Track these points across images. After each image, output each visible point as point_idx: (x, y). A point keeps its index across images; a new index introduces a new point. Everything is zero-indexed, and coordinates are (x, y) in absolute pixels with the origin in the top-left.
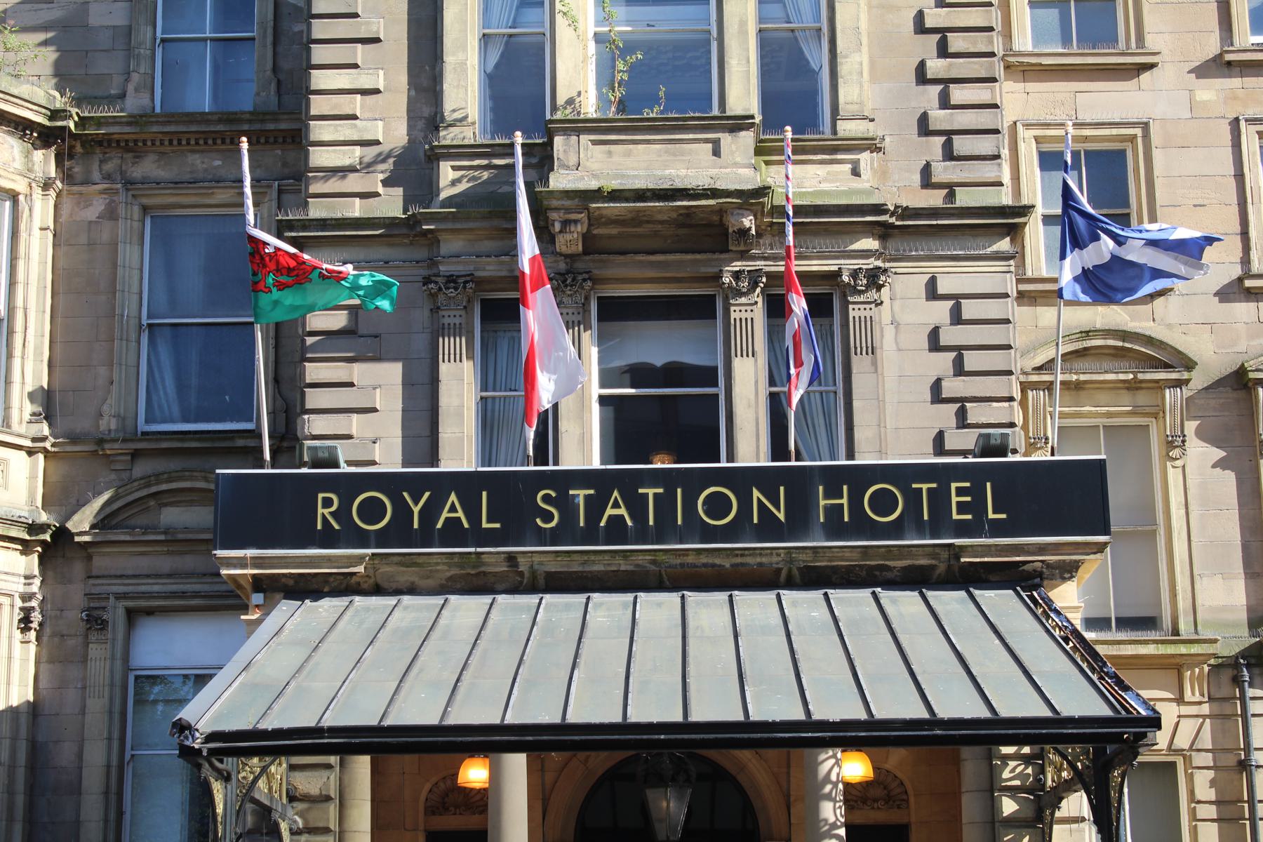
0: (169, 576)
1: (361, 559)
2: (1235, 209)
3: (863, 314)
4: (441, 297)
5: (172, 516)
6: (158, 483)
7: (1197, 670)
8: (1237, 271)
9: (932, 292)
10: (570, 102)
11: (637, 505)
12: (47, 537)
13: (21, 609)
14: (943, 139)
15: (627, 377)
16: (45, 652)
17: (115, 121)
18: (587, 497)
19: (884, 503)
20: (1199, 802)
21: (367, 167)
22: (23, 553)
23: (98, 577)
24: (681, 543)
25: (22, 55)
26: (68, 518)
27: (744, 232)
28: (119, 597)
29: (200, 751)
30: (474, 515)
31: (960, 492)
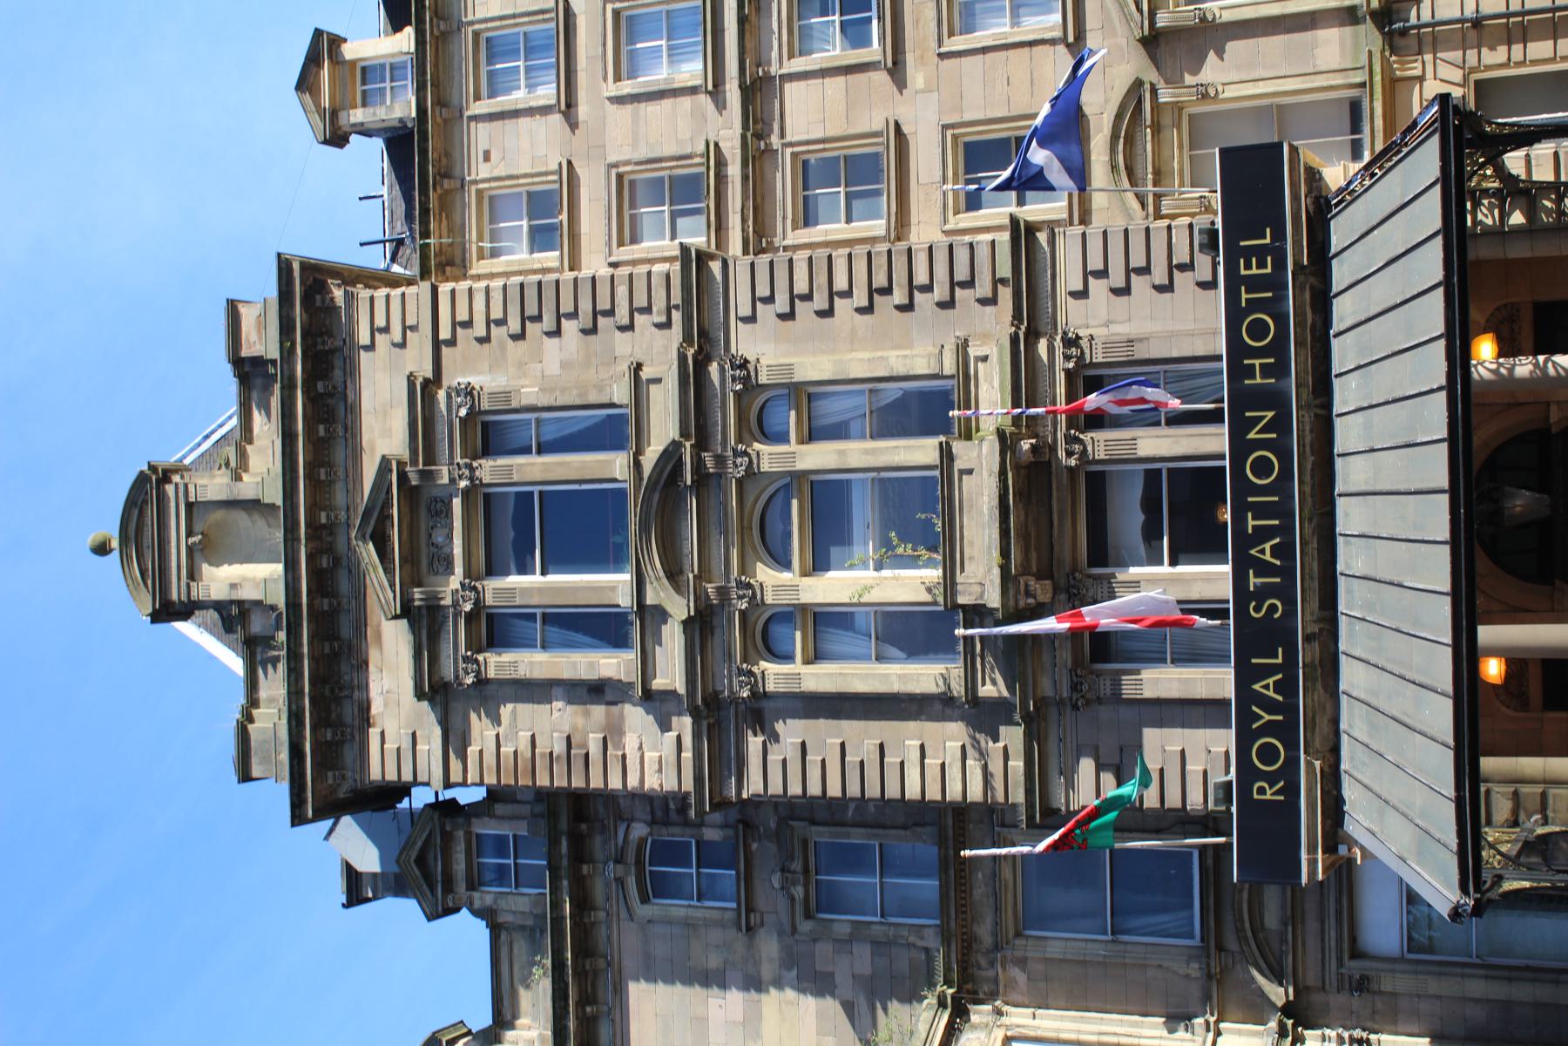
0: (1323, 923)
2: (1011, 53)
3: (1100, 351)
4: (1089, 696)
5: (1272, 920)
6: (1244, 930)
7: (1395, 66)
8: (1061, 49)
9: (1082, 294)
10: (929, 590)
11: (1262, 534)
12: (1290, 1022)
15: (1154, 543)
18: (1256, 576)
20: (1509, 59)
21: (983, 755)
25: (895, 1029)
26: (1273, 1005)
27: (1034, 448)
28: (1340, 964)
29: (1476, 900)
30: (1270, 670)
31: (1248, 266)
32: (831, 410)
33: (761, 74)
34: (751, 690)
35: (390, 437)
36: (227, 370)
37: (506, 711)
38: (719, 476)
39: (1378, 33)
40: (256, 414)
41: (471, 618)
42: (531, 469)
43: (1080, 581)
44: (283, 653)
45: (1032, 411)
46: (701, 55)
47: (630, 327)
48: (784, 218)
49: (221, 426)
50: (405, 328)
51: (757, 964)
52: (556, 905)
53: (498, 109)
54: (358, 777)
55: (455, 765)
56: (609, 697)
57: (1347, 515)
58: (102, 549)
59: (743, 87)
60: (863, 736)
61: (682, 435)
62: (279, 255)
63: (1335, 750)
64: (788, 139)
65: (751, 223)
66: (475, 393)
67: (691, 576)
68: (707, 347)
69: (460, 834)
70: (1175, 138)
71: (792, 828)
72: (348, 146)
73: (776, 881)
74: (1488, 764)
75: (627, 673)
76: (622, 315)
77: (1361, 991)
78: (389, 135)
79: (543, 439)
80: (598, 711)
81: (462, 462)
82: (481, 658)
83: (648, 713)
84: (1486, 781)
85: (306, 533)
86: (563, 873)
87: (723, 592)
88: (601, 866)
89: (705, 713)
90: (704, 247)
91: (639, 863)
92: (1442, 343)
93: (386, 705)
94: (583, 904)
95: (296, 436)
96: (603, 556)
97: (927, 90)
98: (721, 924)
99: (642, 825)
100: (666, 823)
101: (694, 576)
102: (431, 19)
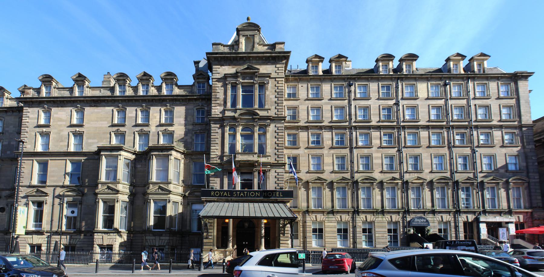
9: (276, 172)
11: (244, 194)
27: (256, 165)
30: (227, 194)
32: (262, 138)
36: (274, 42)
42: (257, 93)
52: (195, 96)
58: (248, 19)
59: (308, 126)
60: (219, 141)
69: (205, 81)
70: (343, 185)
73: (199, 128)
80: (222, 103)
87: (238, 122)
91: (202, 108)
96: (244, 104)
97: (304, 152)
98: (193, 120)
100: (207, 113)
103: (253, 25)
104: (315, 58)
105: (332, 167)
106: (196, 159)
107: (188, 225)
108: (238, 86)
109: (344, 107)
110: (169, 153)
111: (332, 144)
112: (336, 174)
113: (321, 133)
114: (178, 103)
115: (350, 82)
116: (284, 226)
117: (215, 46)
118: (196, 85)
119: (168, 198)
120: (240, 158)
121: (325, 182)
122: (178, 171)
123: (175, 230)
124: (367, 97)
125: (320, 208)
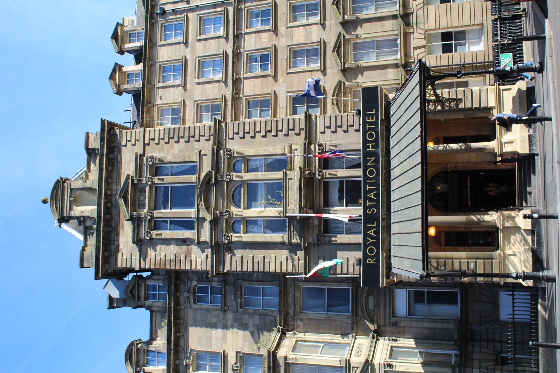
0: (385, 307)
1: (382, 253)
3: (328, 148)
4: (322, 242)
5: (371, 306)
6: (363, 309)
8: (320, 72)
9: (323, 133)
10: (279, 214)
11: (371, 191)
12: (375, 335)
13: (392, 341)
14: (290, 131)
15: (341, 201)
16: (402, 336)
17: (280, 318)
18: (369, 202)
19: (371, 136)
21: (293, 260)
22: (379, 341)
23: (385, 324)
24: (379, 180)
25: (265, 339)
26: (371, 330)
27: (309, 173)
28: (390, 318)
29: (427, 273)
30: (373, 228)
31: (369, 119)
32: (253, 164)
33: (238, 77)
34: (228, 241)
35: (130, 170)
36: (85, 151)
37: (158, 247)
38: (222, 181)
39: (403, 70)
40: (92, 164)
41: (150, 221)
42: (168, 179)
43: (321, 210)
44: (95, 231)
45: (309, 155)
46: (222, 72)
47: (199, 141)
48: (243, 116)
49: (81, 170)
50: (136, 140)
51: (226, 321)
52: (170, 304)
53: (165, 85)
54: (114, 266)
55: (143, 263)
56: (188, 244)
57: (394, 185)
58: (45, 202)
59: (233, 80)
60: (259, 254)
61: (212, 169)
62: (102, 119)
63: (390, 250)
64: (245, 95)
65: (233, 117)
66: (154, 158)
67: (212, 208)
68: (220, 146)
69: (143, 284)
70: (350, 48)
71: (238, 282)
72: (122, 95)
73: (233, 297)
74: (430, 254)
75: (193, 236)
76: (197, 137)
77: (395, 326)
78: (134, 93)
79: (172, 173)
80: (184, 247)
81: (149, 177)
82: (152, 232)
83: (199, 248)
84: (430, 258)
85: (104, 196)
86: (172, 294)
87: (221, 213)
88: (183, 293)
89: (215, 247)
90: (220, 119)
91: (194, 293)
92: (420, 192)
93: (124, 246)
94: (177, 304)
95: (103, 169)
96: (188, 204)
97: (283, 83)
98: (216, 310)
99: (195, 281)
100: (202, 281)
101: (214, 209)
102: (148, 61)
103: (55, 191)
104: (114, 80)
105: (313, 26)
106: (295, 305)
107: (444, 325)
108: (155, 216)
109: (200, 18)
110: (281, 362)
111: (269, 30)
112: (328, 17)
113: (247, 54)
114: (182, 341)
115: (157, 14)
116: (439, 100)
117: (85, 262)
118: (149, 302)
119: (383, 369)
120: (294, 210)
121: (344, 36)
122: (322, 345)
123: (456, 355)
124: (183, 22)
125: (399, 42)
